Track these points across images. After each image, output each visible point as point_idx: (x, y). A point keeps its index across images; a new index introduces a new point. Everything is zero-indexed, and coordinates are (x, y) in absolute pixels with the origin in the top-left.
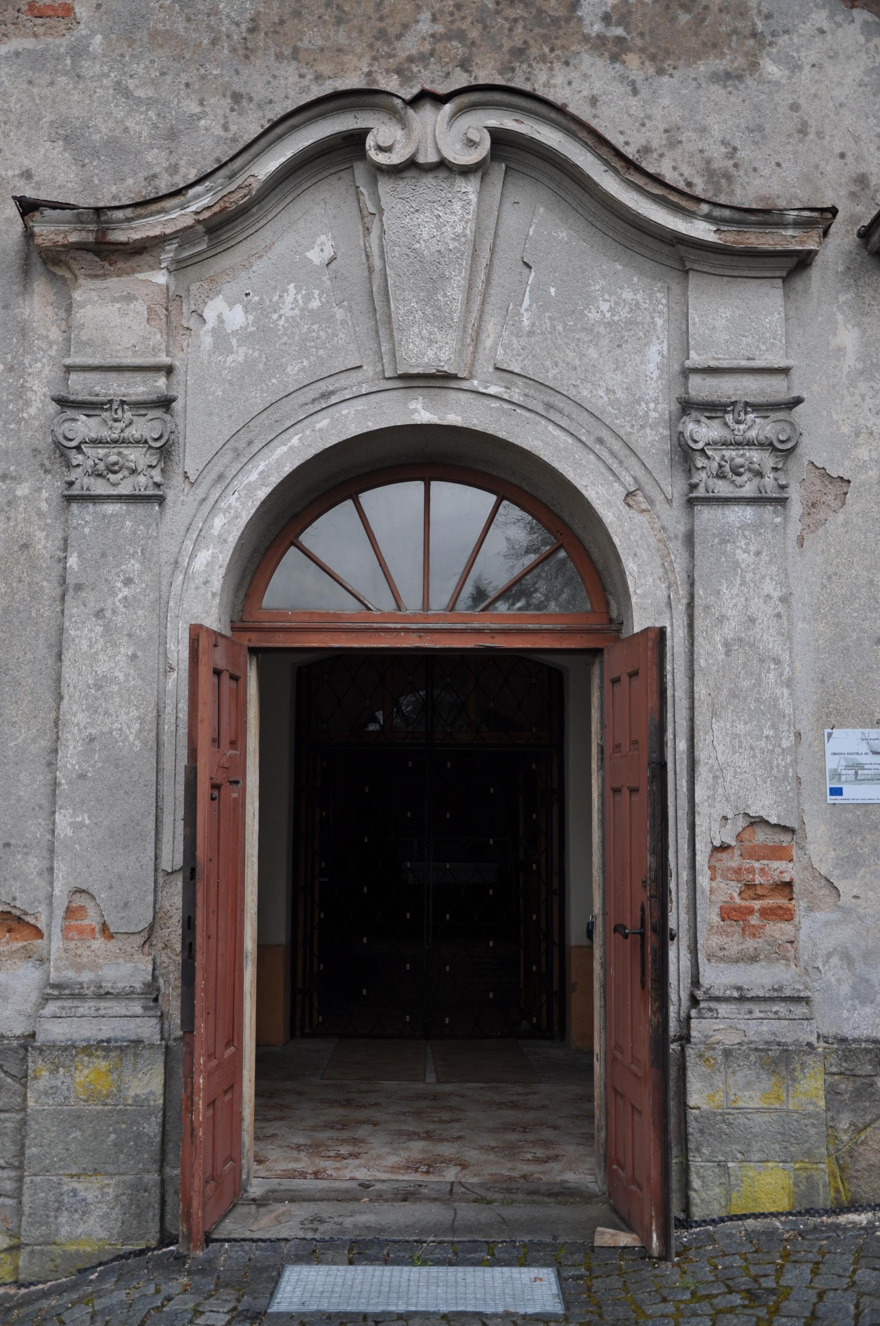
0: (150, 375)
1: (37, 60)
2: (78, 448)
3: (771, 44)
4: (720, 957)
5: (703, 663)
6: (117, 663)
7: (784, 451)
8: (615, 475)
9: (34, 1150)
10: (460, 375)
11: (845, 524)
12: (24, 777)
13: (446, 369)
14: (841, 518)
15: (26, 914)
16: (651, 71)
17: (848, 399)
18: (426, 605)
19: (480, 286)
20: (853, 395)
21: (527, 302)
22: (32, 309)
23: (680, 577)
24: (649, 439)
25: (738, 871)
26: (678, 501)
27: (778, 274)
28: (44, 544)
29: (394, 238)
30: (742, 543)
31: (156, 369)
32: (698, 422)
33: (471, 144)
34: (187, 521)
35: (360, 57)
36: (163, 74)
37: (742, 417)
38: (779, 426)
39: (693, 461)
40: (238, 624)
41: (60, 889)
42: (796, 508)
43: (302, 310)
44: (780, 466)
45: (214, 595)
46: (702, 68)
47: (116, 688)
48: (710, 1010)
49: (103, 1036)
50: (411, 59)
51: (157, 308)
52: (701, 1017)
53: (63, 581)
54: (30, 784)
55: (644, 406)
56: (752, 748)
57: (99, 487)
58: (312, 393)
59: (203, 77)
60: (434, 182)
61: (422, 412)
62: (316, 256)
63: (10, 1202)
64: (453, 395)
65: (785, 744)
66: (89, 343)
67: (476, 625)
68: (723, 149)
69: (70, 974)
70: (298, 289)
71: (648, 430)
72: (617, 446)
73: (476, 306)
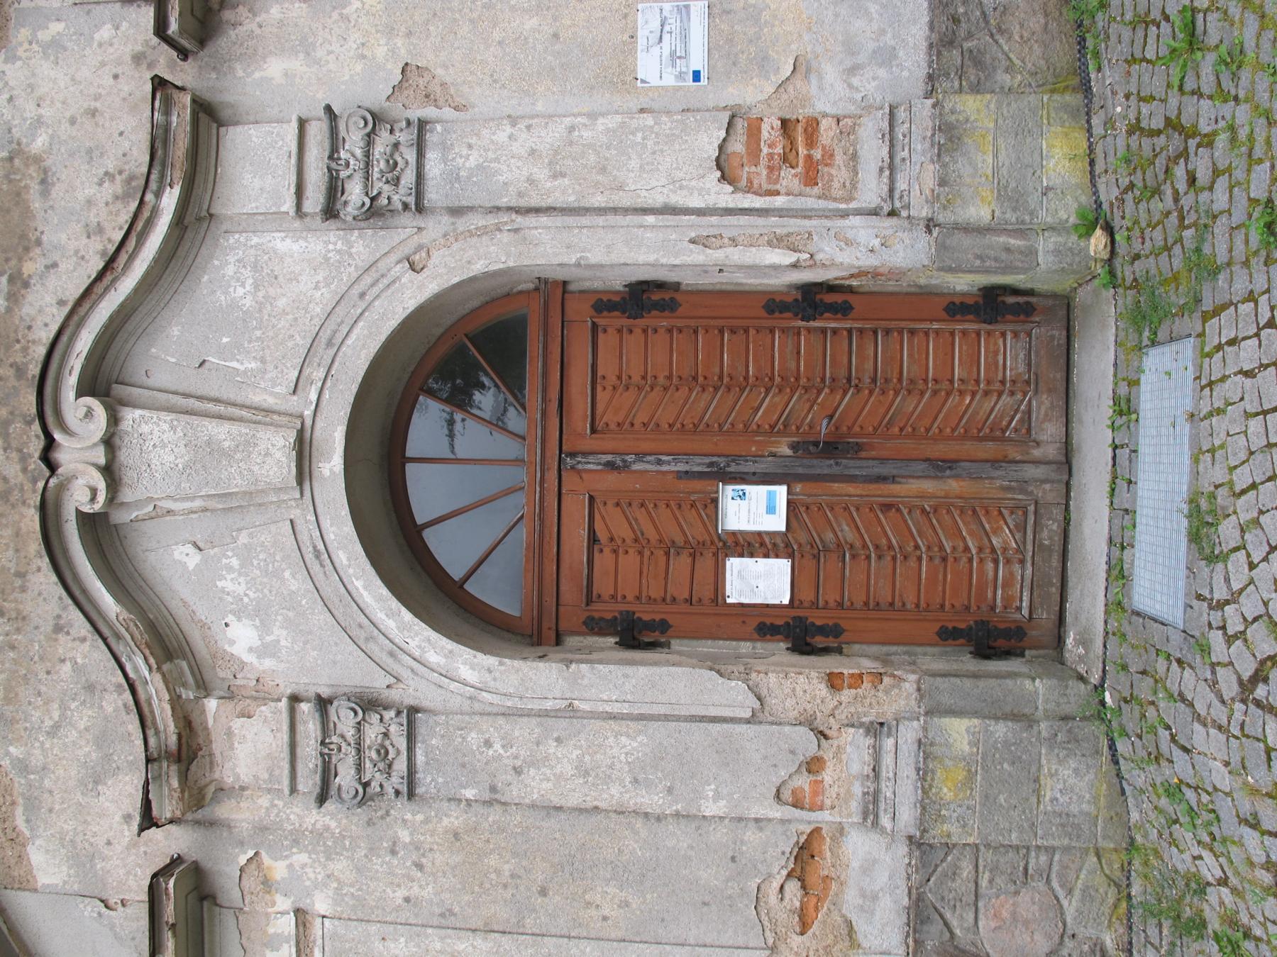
0: (298, 717)
1: (32, 806)
2: (366, 785)
3: (19, 144)
4: (852, 188)
5: (572, 199)
6: (564, 756)
7: (376, 120)
8: (394, 282)
9: (1014, 836)
10: (299, 427)
11: (446, 67)
12: (670, 843)
13: (292, 441)
14: (440, 72)
15: (797, 843)
16: (38, 251)
17: (332, 66)
18: (518, 461)
19: (221, 409)
20: (328, 62)
21: (234, 364)
22: (243, 820)
23: (491, 220)
24: (361, 249)
25: (771, 169)
26: (420, 221)
27: (214, 131)
28: (454, 819)
29: (173, 488)
30: (461, 161)
31: (292, 712)
32: (346, 203)
33: (89, 414)
34: (433, 687)
35: (23, 516)
36: (39, 694)
37: (342, 162)
38: (352, 128)
39: (381, 208)
40: (535, 639)
41: (777, 812)
42: (429, 112)
43: (240, 574)
44: (389, 127)
45: (501, 664)
46: (36, 204)
47: (587, 758)
48: (901, 197)
49: (913, 775)
50: (25, 470)
51: (238, 709)
52: (908, 207)
53: (489, 803)
54: (678, 838)
55: (330, 255)
56: (654, 153)
57: (401, 766)
58: (315, 568)
59: (41, 659)
60: (124, 450)
61: (332, 463)
62: (192, 559)
63: (1057, 857)
64: (317, 433)
65: (650, 122)
66: (270, 771)
67: (539, 416)
68: (106, 185)
69: (855, 806)
70: (222, 578)
71: (354, 250)
72: (368, 280)
73: (232, 411)
